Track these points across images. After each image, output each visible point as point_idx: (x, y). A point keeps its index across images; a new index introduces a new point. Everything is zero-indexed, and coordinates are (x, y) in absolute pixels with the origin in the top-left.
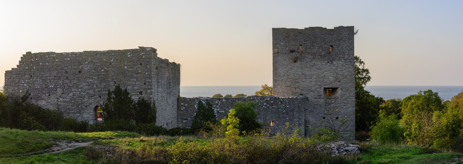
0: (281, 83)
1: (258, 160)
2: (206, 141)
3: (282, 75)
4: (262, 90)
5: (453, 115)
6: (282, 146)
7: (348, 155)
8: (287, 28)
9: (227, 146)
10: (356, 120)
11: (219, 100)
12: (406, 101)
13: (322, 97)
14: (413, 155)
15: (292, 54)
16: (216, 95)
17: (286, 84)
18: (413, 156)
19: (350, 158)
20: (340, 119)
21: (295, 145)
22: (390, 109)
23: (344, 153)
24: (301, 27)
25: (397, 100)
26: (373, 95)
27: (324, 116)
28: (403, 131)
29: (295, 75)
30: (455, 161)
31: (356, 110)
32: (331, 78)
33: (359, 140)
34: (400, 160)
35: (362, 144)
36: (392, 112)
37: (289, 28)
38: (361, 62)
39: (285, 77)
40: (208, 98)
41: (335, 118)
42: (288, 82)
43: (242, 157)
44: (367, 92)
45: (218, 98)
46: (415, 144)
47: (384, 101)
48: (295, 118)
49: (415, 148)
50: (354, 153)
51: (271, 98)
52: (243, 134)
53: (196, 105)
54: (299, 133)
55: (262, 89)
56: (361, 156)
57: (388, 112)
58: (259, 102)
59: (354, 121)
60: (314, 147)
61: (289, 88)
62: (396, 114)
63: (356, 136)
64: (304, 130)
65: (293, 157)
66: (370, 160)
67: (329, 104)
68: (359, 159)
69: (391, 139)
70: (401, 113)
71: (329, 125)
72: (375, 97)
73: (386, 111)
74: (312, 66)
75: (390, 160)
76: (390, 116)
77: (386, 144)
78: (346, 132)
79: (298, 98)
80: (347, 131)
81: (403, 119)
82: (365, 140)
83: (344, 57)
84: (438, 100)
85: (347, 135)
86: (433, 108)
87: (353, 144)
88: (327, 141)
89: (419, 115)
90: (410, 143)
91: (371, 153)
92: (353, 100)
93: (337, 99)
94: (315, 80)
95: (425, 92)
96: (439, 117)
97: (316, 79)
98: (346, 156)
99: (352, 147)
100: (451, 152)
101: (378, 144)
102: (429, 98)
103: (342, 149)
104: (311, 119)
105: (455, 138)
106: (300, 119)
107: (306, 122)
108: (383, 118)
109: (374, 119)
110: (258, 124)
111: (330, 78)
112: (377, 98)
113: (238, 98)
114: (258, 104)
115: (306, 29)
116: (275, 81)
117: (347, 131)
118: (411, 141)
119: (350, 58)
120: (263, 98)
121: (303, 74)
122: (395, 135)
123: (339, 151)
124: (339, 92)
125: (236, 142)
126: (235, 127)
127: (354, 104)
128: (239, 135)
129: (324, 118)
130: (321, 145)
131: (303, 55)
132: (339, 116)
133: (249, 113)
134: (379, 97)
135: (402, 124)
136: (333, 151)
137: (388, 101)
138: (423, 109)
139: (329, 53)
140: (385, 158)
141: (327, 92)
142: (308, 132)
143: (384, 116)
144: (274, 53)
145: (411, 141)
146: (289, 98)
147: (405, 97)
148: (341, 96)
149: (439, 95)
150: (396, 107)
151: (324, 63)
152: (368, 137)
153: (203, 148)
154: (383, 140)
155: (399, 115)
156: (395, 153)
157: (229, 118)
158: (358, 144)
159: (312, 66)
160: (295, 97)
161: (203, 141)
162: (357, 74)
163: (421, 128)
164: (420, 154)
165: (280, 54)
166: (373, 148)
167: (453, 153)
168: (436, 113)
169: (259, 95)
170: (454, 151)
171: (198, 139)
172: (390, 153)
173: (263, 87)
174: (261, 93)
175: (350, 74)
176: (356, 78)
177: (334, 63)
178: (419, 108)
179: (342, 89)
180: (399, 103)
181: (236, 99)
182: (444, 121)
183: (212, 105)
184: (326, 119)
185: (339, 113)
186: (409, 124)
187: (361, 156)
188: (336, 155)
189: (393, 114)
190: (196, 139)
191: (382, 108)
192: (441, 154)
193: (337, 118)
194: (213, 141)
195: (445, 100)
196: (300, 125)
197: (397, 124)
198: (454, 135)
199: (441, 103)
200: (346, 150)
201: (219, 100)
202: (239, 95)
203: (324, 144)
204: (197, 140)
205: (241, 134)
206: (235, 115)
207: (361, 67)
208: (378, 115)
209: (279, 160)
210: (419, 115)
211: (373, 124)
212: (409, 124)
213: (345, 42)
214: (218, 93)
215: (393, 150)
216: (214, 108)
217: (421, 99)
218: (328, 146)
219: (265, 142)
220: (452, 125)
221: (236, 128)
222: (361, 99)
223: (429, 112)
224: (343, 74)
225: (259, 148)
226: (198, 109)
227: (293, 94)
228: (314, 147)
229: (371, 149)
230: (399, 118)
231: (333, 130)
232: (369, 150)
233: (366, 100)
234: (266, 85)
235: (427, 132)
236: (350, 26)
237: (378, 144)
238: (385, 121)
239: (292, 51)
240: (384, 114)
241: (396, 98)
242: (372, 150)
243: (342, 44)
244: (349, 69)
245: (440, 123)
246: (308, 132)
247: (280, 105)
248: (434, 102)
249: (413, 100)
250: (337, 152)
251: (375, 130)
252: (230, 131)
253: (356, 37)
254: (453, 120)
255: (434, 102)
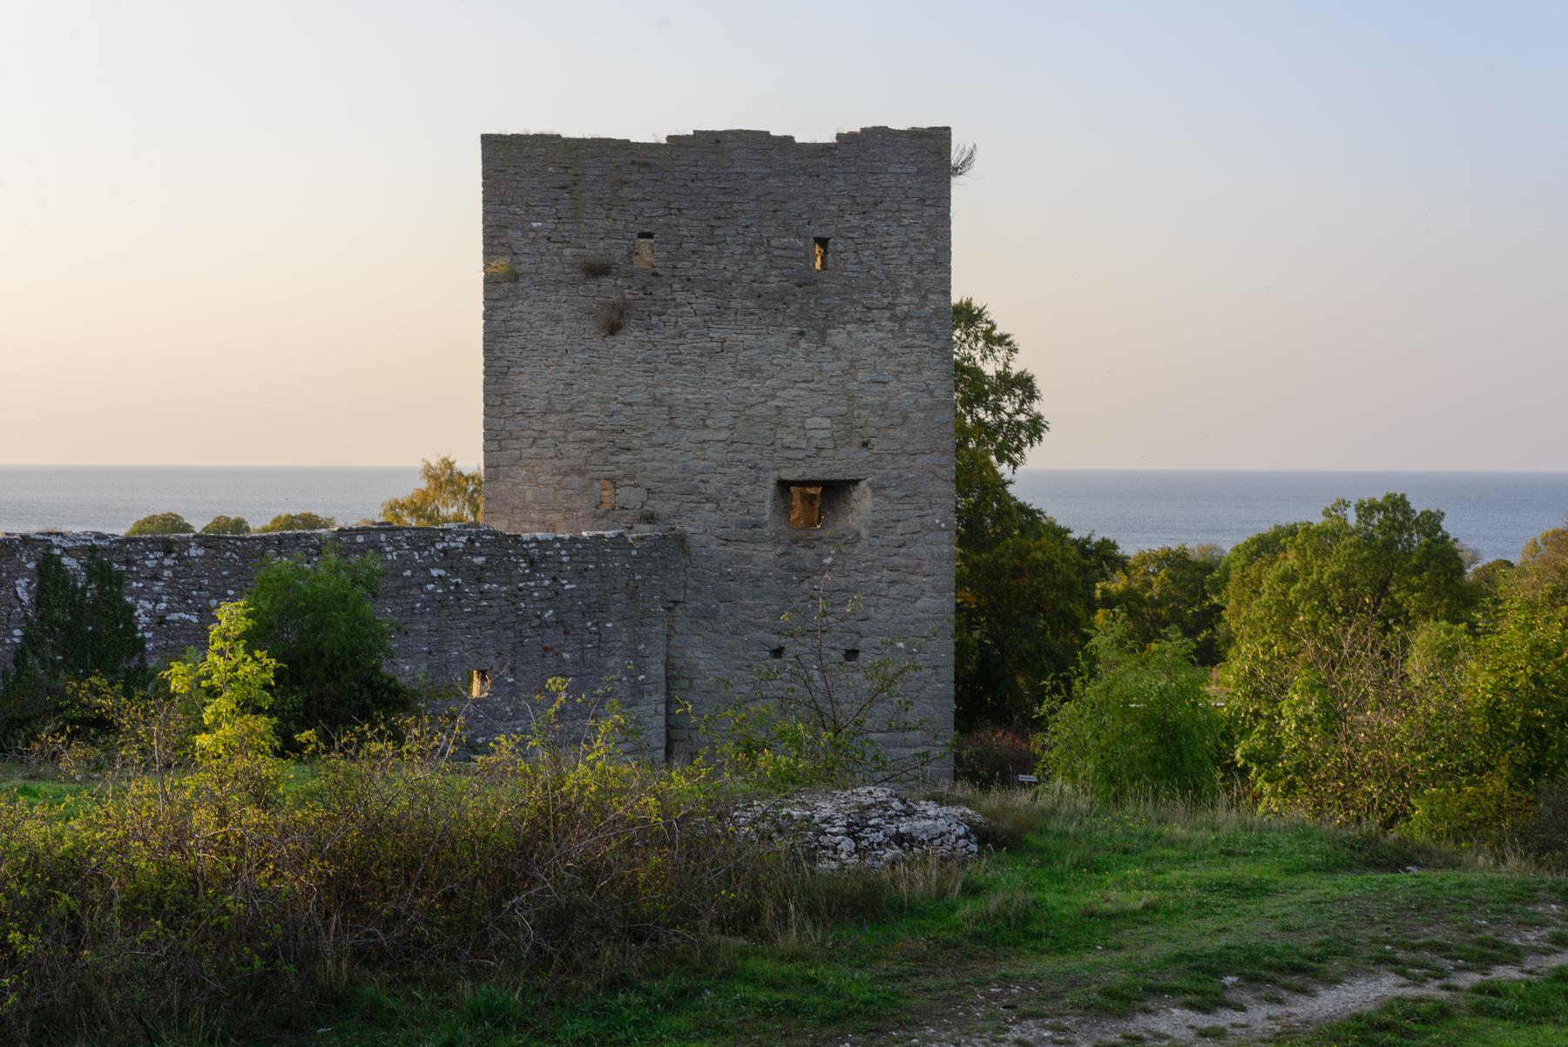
0: (528, 452)
1: (387, 897)
2: (75, 793)
3: (538, 403)
4: (425, 494)
5: (1536, 647)
6: (529, 813)
7: (909, 864)
8: (566, 134)
9: (203, 819)
10: (958, 667)
11: (167, 547)
12: (1250, 561)
13: (766, 531)
14: (1289, 872)
15: (592, 284)
16: (140, 524)
17: (559, 455)
18: (1284, 880)
19: (920, 882)
20: (867, 659)
21: (600, 807)
22: (1158, 605)
23: (889, 854)
24: (647, 125)
25: (1195, 555)
26: (1061, 523)
27: (776, 641)
28: (1230, 732)
29: (614, 406)
30: (1543, 925)
31: (959, 608)
32: (821, 428)
33: (973, 777)
34: (1212, 899)
35: (994, 799)
36: (1166, 625)
37: (579, 135)
38: (995, 340)
39: (552, 418)
40: (100, 536)
41: (837, 656)
42: (570, 449)
43: (291, 883)
44: (1023, 509)
45: (164, 537)
46: (1301, 812)
47: (1121, 564)
48: (610, 655)
49: (1302, 833)
50: (944, 850)
51: (475, 536)
52: (298, 748)
53: (22, 583)
54: (629, 736)
55: (423, 484)
56: (981, 870)
57: (1146, 623)
58: (406, 562)
59: (949, 672)
60: (720, 817)
61: (576, 480)
62: (1190, 632)
63: (958, 760)
64: (661, 720)
65: (590, 874)
66: (1034, 896)
67: (804, 574)
68: (972, 890)
69: (1157, 776)
70: (1221, 628)
71: (802, 692)
72: (1075, 535)
73: (1132, 614)
74: (712, 354)
75: (1149, 896)
76: (1154, 646)
77: (1130, 809)
78: (898, 736)
79: (630, 537)
80: (906, 728)
81: (1235, 665)
82: (1007, 782)
83: (891, 307)
84: (1442, 559)
85: (907, 752)
86: (1412, 603)
87: (940, 800)
88: (789, 781)
89: (1329, 640)
90: (1270, 804)
91: (1046, 858)
92: (939, 551)
93: (853, 544)
94: (724, 435)
95: (1367, 510)
96: (1448, 655)
97: (731, 428)
98: (901, 868)
99: (934, 820)
100: (1515, 868)
101: (1082, 803)
102: (1388, 546)
103: (877, 828)
104: (702, 659)
105: (1543, 784)
106: (641, 662)
107: (673, 676)
108: (1113, 656)
109: (1061, 663)
110: (396, 691)
111: (809, 423)
112: (1082, 546)
113: (281, 540)
114: (398, 575)
115: (677, 142)
116: (495, 437)
117: (906, 728)
118: (1274, 794)
119: (928, 310)
120: (425, 538)
121: (656, 402)
122: (1182, 758)
123: (855, 839)
124: (864, 503)
125: (261, 797)
126: (248, 706)
127: (946, 575)
128: (279, 754)
129: (778, 652)
130: (759, 807)
131: (659, 293)
132: (863, 643)
133: (337, 623)
134: (1096, 539)
135: (1222, 690)
136: (825, 840)
137: (1144, 559)
138: (1351, 607)
139: (807, 281)
140: (1123, 884)
141: (797, 501)
142: (682, 734)
143: (1121, 643)
144: (491, 282)
145: (1274, 794)
146: (574, 540)
147: (1242, 539)
148: (877, 529)
149: (1447, 525)
150: (1192, 593)
151: (778, 339)
152: (1026, 763)
153: (59, 837)
154: (1113, 784)
155: (1210, 642)
156: (1182, 861)
157: (212, 658)
158: (967, 803)
159: (712, 354)
160: (610, 533)
161: (58, 797)
162: (968, 403)
163: (1341, 716)
164: (1329, 868)
165: (524, 283)
166: (1054, 825)
167: (1532, 876)
168: (1428, 635)
169: (411, 521)
170: (1540, 864)
171: (34, 785)
172: (1149, 861)
173: (430, 474)
174: (416, 510)
175: (925, 400)
176: (963, 434)
177: (837, 337)
178: (1325, 602)
179: (877, 489)
180: (1209, 569)
181: (266, 541)
182: (1478, 681)
183: (119, 580)
184: (789, 655)
185: (863, 626)
186: (1266, 691)
187: (981, 870)
188: (843, 866)
189: (1174, 632)
190: (18, 782)
191: (1109, 601)
192: (1452, 877)
193: (852, 654)
194: (119, 796)
195: (1487, 559)
196: (638, 691)
197: (1192, 691)
198: (1537, 770)
199: (1460, 571)
200: (900, 839)
201: (168, 552)
202: (290, 522)
203: (777, 798)
204: (25, 791)
205: (288, 748)
206: (251, 641)
207: (990, 368)
208: (1087, 638)
209: (508, 894)
210: (1329, 640)
211: (1056, 690)
212: (1266, 691)
213: (898, 220)
214: (161, 509)
215: (1172, 844)
216: (138, 594)
217: (1341, 550)
218: (796, 813)
219: (427, 789)
220: (1528, 707)
221: (258, 711)
222: (987, 546)
223: (1386, 629)
224: (884, 406)
225: (397, 827)
226: (38, 603)
227: (601, 514)
228: (720, 817)
229: (1042, 832)
230: (1210, 656)
231: (821, 717)
232: (1033, 838)
233: (1022, 554)
234: (450, 465)
235: (1373, 745)
236: (925, 124)
237: (1082, 803)
238: (1123, 676)
239: (596, 271)
240: (1118, 630)
241: (1194, 543)
242: (1050, 841)
243: (881, 228)
244: (919, 371)
245: (1453, 694)
246: (682, 734)
247: (527, 578)
248: (1418, 570)
249: (1292, 554)
250: (847, 844)
251: (1067, 721)
252: (222, 731)
253: (959, 189)
254: (1536, 679)
255: (1418, 570)
